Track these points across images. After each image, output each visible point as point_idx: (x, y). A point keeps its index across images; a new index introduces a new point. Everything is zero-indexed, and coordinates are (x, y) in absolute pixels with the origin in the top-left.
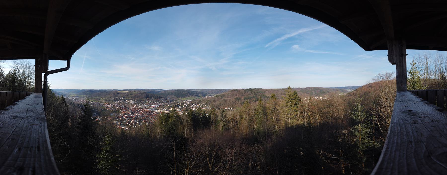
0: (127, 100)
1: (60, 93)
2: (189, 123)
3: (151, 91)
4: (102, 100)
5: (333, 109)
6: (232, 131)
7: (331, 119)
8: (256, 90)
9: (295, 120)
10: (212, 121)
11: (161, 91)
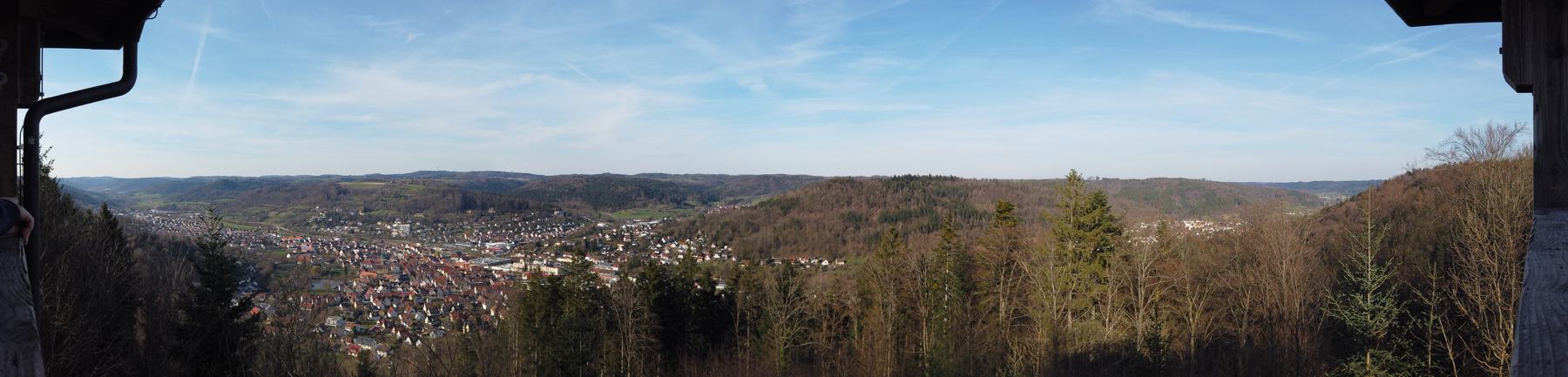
1: (95, 197)
2: (644, 327)
3: (483, 180)
4: (276, 222)
5: (1256, 278)
6: (828, 367)
7: (1249, 324)
8: (934, 185)
9: (1092, 322)
10: (743, 315)
11: (526, 183)
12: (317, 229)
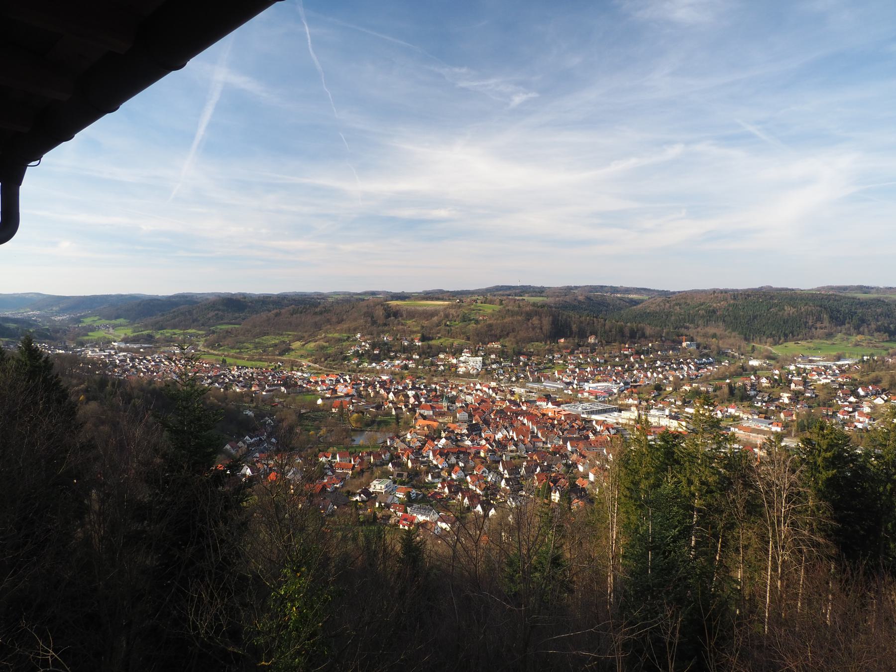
0: (444, 352)
1: (12, 326)
11: (642, 301)
12: (358, 365)
